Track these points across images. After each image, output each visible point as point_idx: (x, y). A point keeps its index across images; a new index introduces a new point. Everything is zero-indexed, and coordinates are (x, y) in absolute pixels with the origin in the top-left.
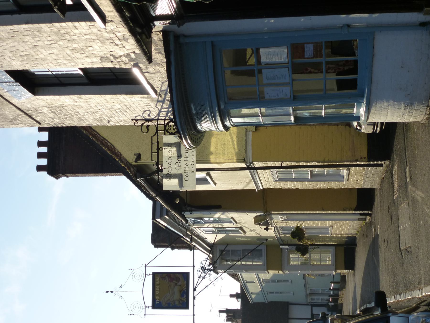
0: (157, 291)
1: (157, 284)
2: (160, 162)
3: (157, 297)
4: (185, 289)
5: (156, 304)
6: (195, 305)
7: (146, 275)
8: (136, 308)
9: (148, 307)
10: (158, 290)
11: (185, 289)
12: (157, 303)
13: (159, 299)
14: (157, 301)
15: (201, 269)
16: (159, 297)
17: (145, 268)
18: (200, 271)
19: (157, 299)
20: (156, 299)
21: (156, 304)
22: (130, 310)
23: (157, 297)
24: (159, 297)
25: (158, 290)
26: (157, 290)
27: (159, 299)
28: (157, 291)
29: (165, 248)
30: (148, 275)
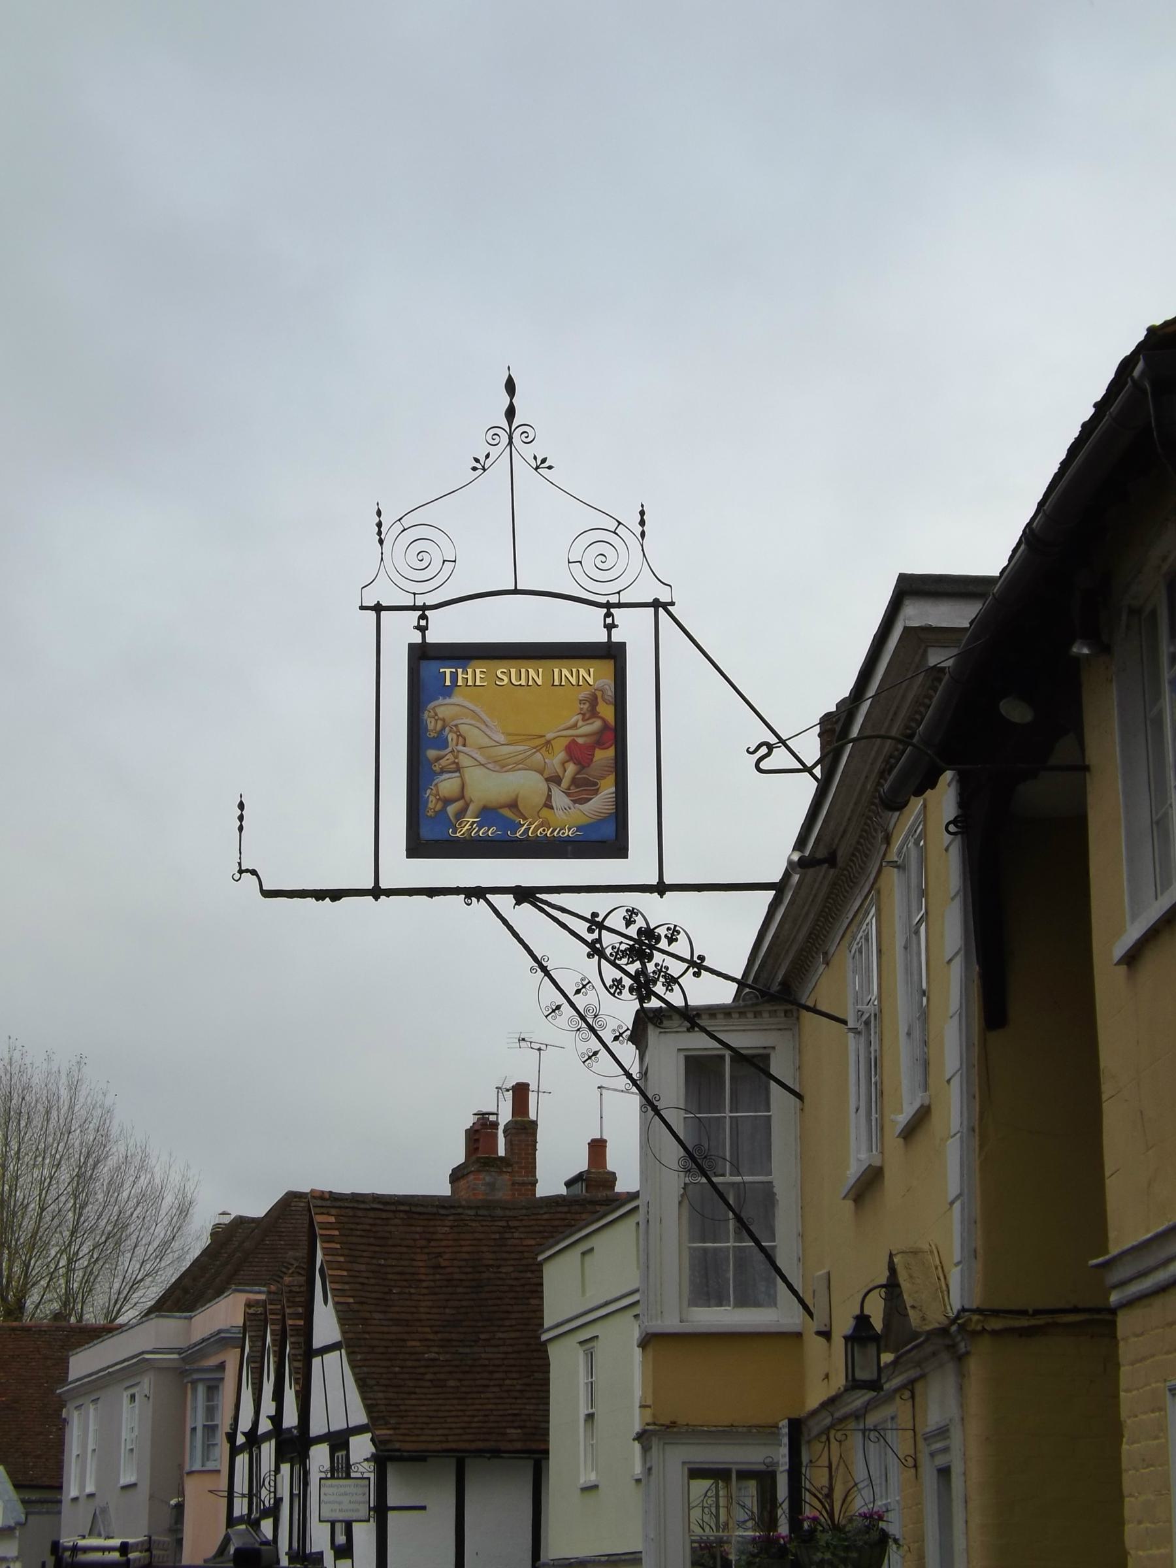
0: (513, 671)
1: (556, 671)
4: (527, 830)
5: (441, 670)
9: (423, 623)
11: (527, 830)
12: (448, 671)
19: (470, 676)
21: (441, 670)
22: (406, 522)
23: (478, 671)
26: (523, 671)
30: (609, 621)
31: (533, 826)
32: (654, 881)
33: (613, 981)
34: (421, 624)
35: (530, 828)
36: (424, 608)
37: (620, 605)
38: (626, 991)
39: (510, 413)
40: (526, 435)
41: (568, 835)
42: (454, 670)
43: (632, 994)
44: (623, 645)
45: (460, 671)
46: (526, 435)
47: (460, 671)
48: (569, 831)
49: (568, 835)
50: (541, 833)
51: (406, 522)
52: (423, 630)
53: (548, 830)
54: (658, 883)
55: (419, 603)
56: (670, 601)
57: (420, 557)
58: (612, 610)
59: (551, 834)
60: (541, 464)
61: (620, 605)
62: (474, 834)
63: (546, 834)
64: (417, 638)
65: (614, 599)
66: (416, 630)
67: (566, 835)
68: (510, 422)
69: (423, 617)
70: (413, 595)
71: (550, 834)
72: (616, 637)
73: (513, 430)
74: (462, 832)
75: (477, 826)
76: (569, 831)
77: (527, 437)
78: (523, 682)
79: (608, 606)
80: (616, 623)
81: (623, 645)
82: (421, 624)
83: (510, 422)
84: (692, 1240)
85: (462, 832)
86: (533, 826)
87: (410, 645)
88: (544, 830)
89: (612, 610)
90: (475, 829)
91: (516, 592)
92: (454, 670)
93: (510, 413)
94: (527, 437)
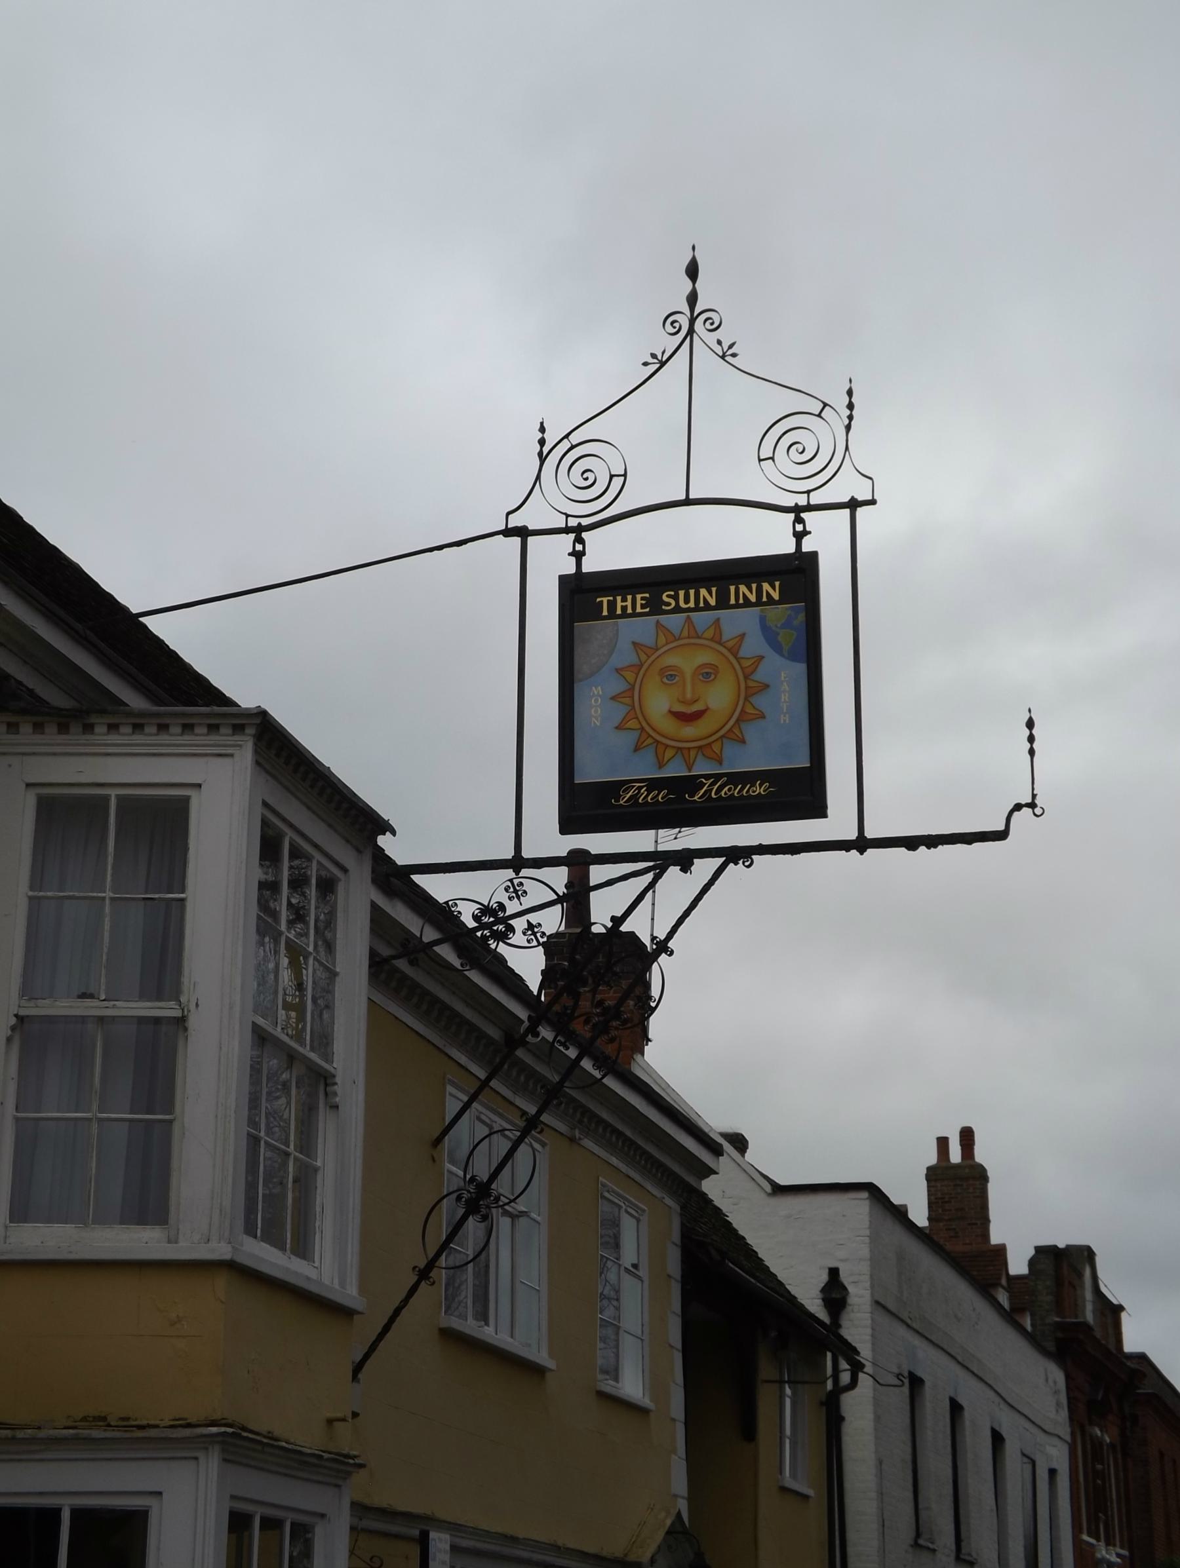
0: (682, 593)
1: (732, 588)
2: (657, 833)
3: (639, 602)
4: (709, 791)
5: (598, 600)
6: (1005, 821)
7: (792, 516)
8: (585, 476)
9: (579, 547)
10: (687, 601)
11: (709, 791)
12: (605, 600)
13: (630, 611)
14: (615, 601)
15: (511, 929)
16: (639, 610)
17: (846, 499)
18: (531, 926)
19: (629, 603)
20: (629, 597)
21: (598, 600)
22: (575, 438)
23: (639, 597)
24: (639, 610)
25: (687, 601)
26: (692, 592)
27: (630, 611)
28: (682, 593)
29: (417, 878)
30: (799, 528)
31: (716, 787)
32: (852, 835)
33: (525, 892)
34: (577, 549)
35: (713, 789)
36: (579, 530)
37: (810, 508)
38: (502, 897)
39: (692, 299)
40: (711, 321)
41: (760, 793)
42: (611, 598)
43: (496, 903)
44: (814, 555)
45: (619, 598)
46: (711, 321)
47: (619, 598)
48: (760, 789)
49: (760, 793)
50: (725, 794)
51: (575, 438)
52: (578, 556)
53: (735, 790)
54: (857, 837)
55: (573, 522)
56: (871, 498)
57: (585, 476)
58: (802, 515)
59: (738, 793)
60: (726, 355)
61: (810, 508)
62: (642, 800)
63: (733, 794)
64: (569, 567)
65: (802, 501)
66: (570, 557)
67: (757, 793)
68: (692, 309)
69: (579, 540)
70: (564, 516)
71: (738, 793)
72: (808, 545)
73: (695, 314)
74: (626, 799)
75: (645, 790)
76: (760, 789)
77: (712, 324)
78: (692, 604)
79: (797, 510)
80: (808, 529)
81: (814, 555)
82: (577, 549)
83: (692, 309)
84: (76, 1513)
85: (626, 799)
86: (716, 787)
87: (562, 579)
88: (730, 790)
89: (802, 515)
90: (643, 794)
91: (688, 502)
92: (611, 598)
93: (692, 299)
94: (712, 324)
